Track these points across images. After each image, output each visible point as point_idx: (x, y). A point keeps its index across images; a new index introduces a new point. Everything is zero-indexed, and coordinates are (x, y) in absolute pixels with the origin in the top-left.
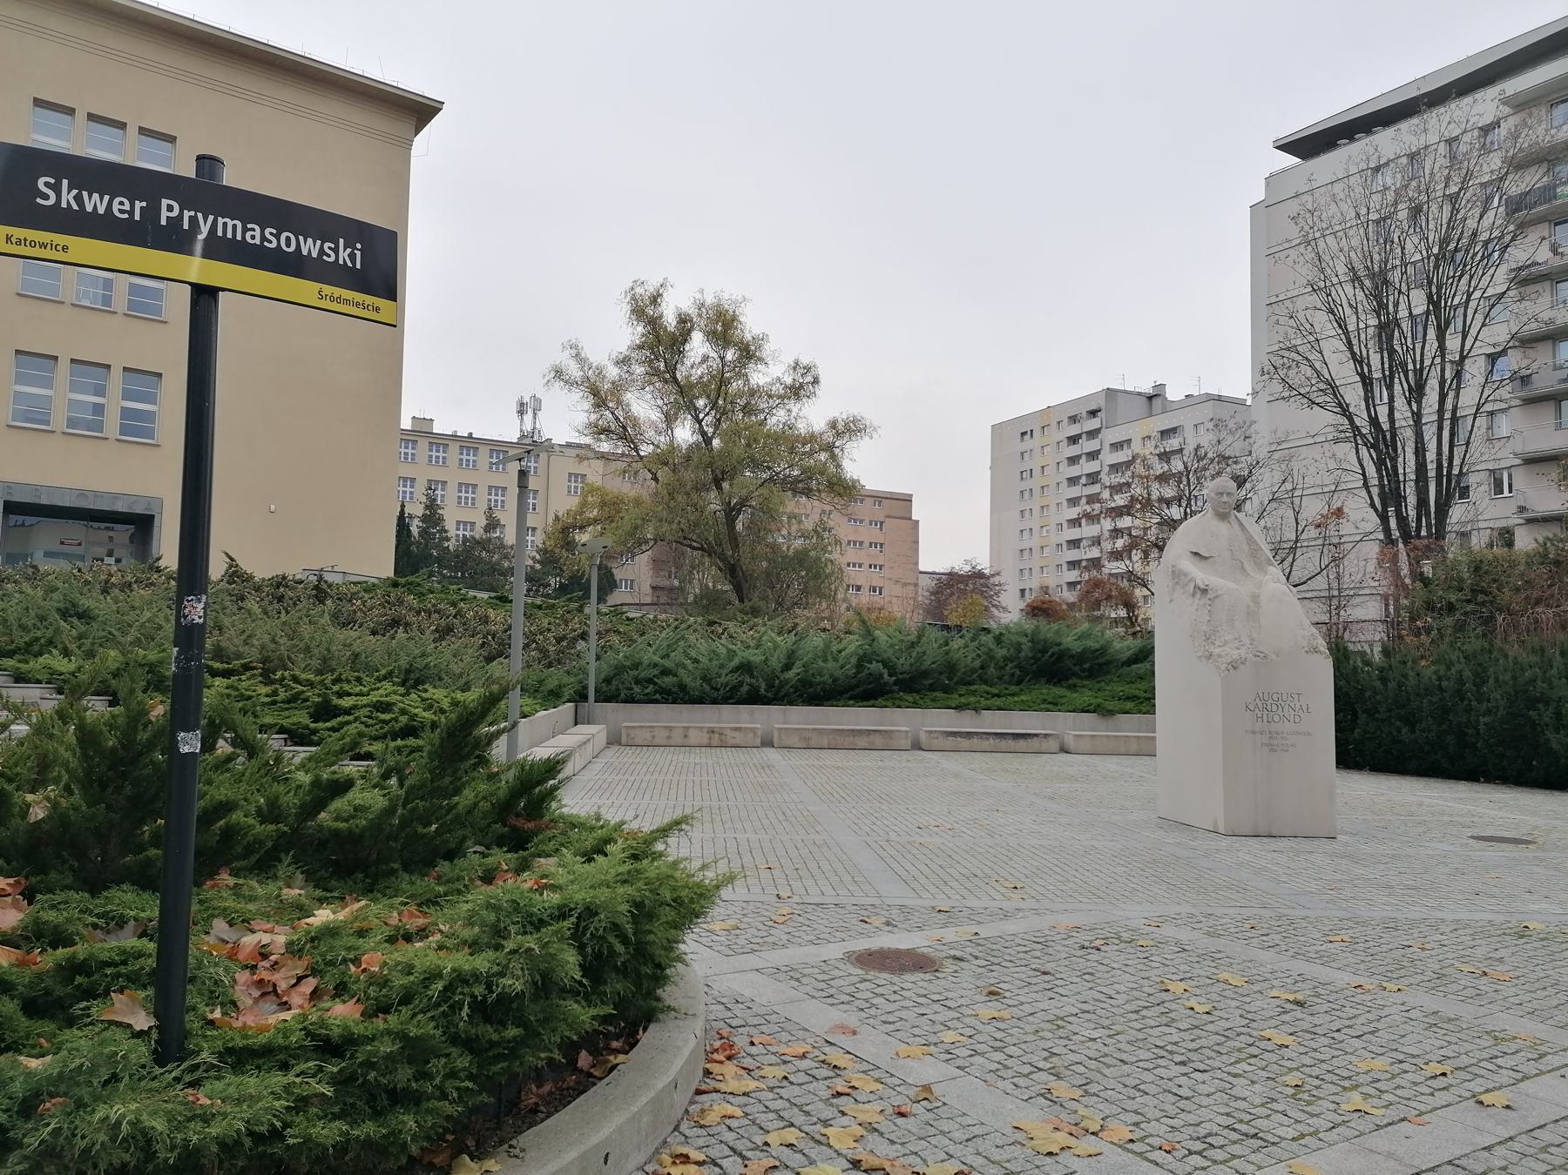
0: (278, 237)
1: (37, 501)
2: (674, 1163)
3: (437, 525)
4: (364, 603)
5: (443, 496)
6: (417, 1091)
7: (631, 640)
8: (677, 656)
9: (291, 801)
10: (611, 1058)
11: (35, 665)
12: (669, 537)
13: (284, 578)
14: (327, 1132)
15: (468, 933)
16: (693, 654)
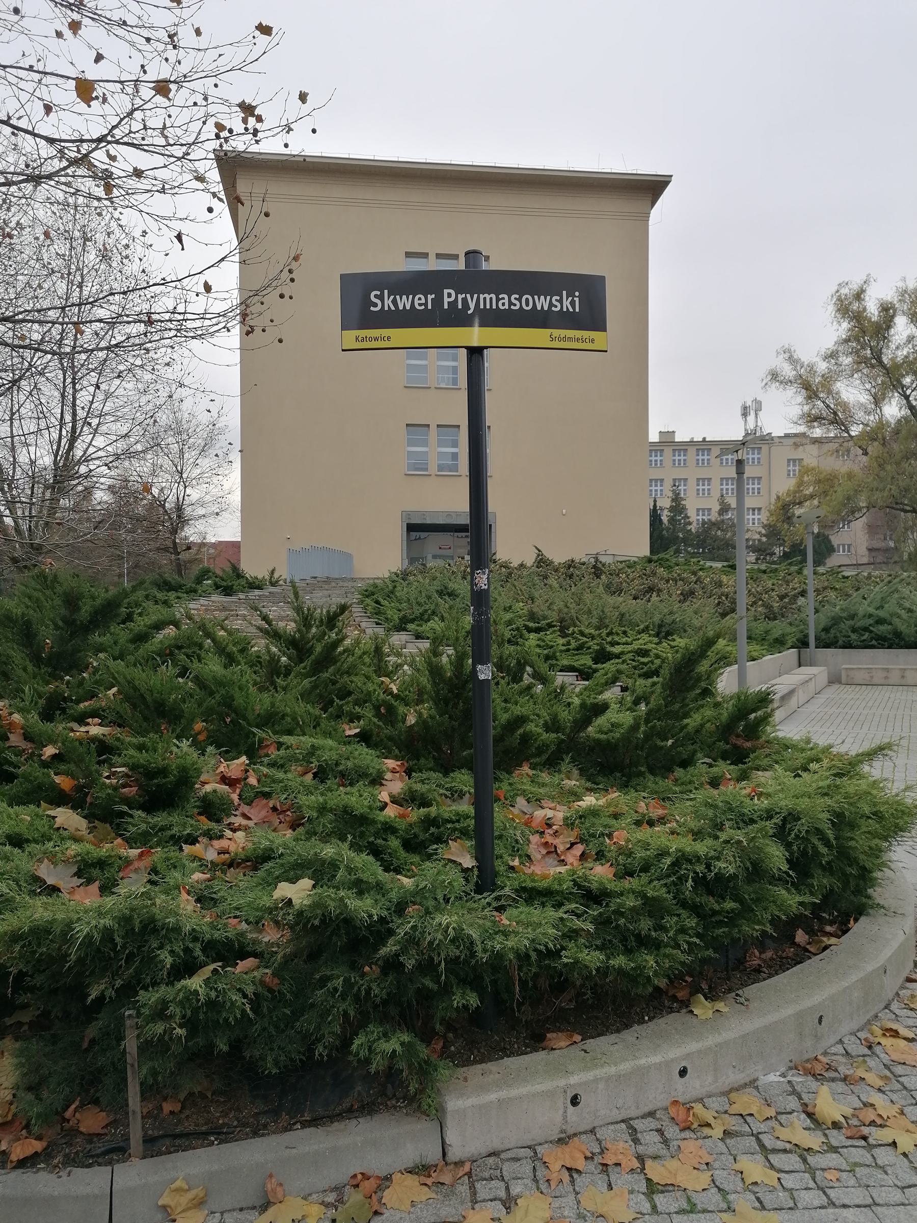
0: (520, 300)
1: (424, 522)
2: (884, 1035)
3: (681, 513)
4: (627, 576)
5: (685, 490)
6: (656, 938)
7: (847, 595)
8: (891, 606)
9: (565, 716)
10: (825, 939)
11: (426, 628)
12: (880, 503)
13: (573, 561)
14: (593, 958)
15: (693, 824)
16: (907, 605)
